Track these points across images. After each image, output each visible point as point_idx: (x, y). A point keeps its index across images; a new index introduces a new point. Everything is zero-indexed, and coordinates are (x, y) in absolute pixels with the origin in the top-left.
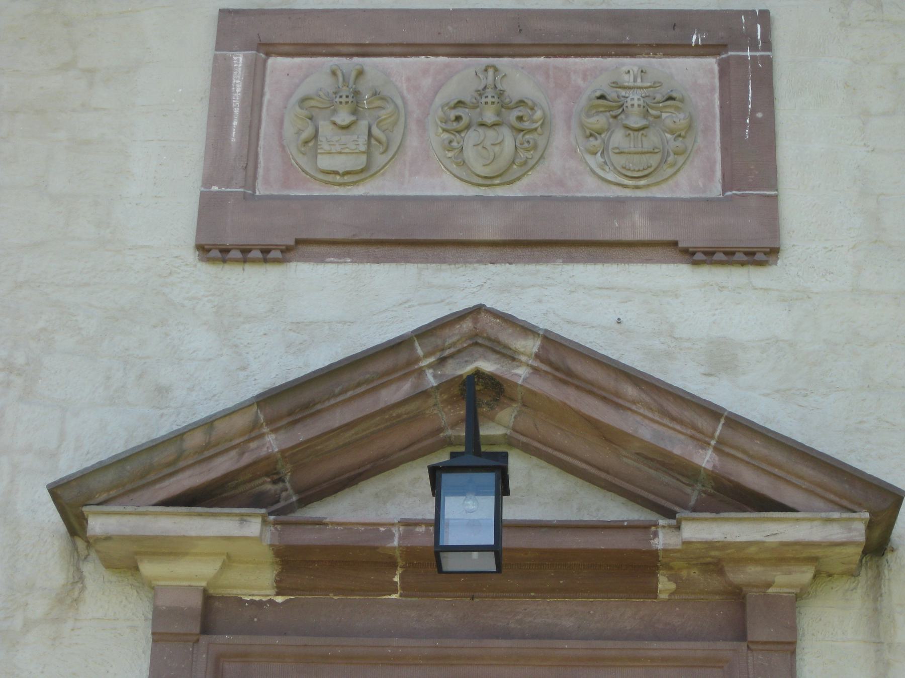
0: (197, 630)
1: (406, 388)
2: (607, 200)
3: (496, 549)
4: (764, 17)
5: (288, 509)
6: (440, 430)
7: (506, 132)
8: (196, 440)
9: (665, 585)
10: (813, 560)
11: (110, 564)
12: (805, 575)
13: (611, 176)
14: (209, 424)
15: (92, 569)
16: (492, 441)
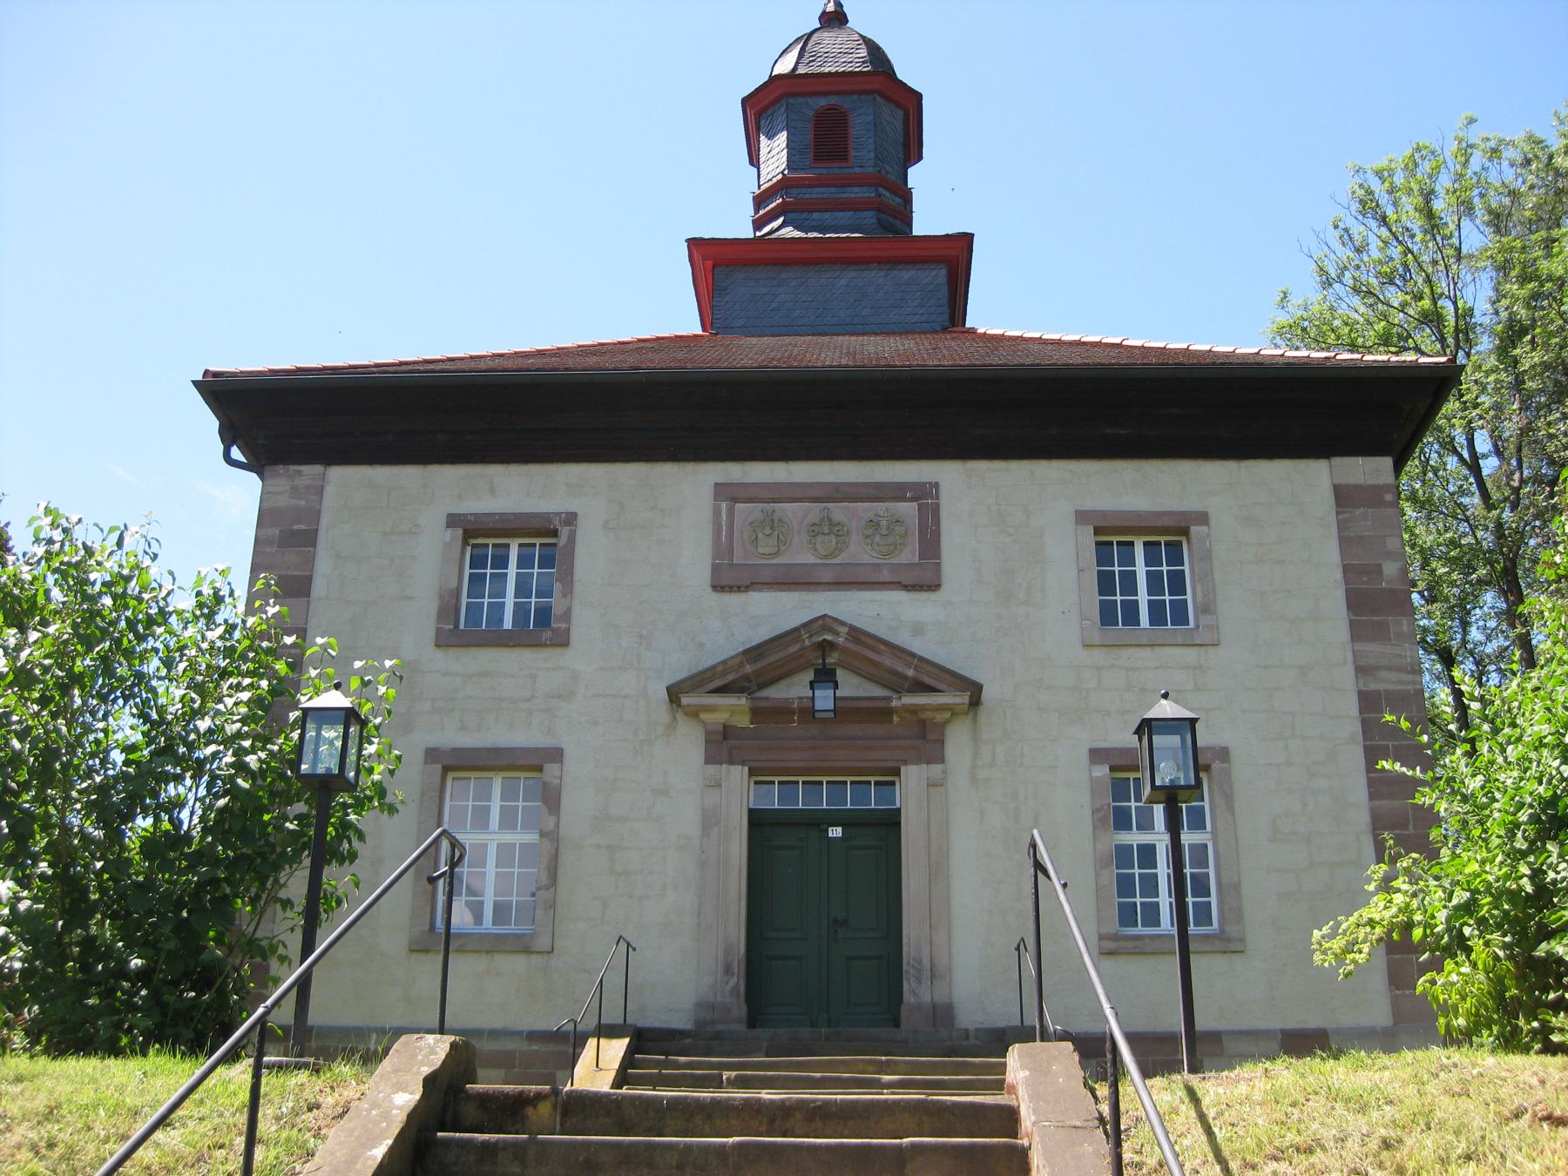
0: (721, 738)
1: (798, 647)
2: (873, 564)
3: (834, 711)
5: (753, 692)
6: (1101, 1119)
7: (833, 537)
8: (720, 668)
9: (896, 719)
10: (950, 709)
11: (686, 714)
12: (947, 715)
13: (875, 555)
14: (724, 662)
15: (680, 716)
16: (830, 664)
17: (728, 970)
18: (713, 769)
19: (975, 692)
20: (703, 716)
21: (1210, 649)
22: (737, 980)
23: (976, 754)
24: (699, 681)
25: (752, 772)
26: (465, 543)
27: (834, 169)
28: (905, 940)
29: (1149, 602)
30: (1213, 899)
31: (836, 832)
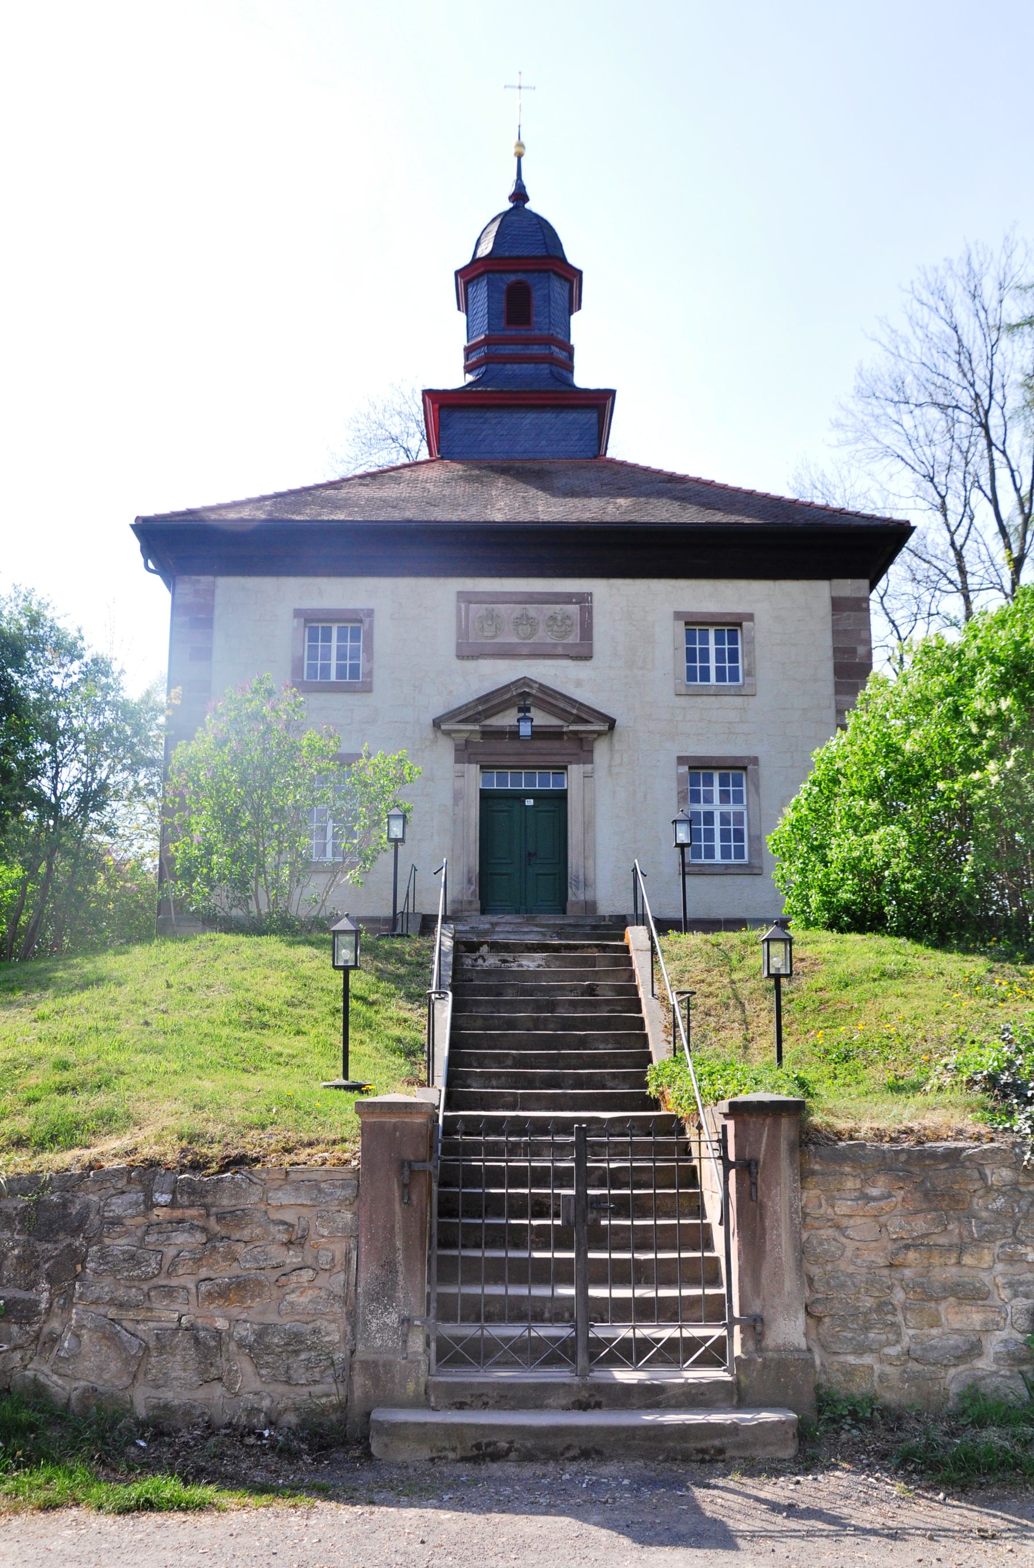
4: (591, 594)
9: (565, 737)
12: (596, 736)
14: (466, 705)
15: (439, 734)
17: (470, 881)
18: (459, 766)
19: (612, 723)
20: (453, 735)
21: (751, 698)
22: (475, 887)
23: (612, 758)
24: (452, 715)
25: (482, 767)
26: (305, 626)
27: (523, 332)
28: (569, 865)
29: (717, 667)
30: (746, 844)
31: (530, 802)
